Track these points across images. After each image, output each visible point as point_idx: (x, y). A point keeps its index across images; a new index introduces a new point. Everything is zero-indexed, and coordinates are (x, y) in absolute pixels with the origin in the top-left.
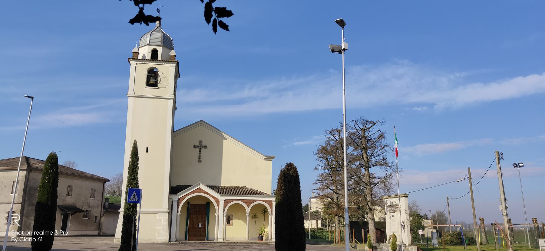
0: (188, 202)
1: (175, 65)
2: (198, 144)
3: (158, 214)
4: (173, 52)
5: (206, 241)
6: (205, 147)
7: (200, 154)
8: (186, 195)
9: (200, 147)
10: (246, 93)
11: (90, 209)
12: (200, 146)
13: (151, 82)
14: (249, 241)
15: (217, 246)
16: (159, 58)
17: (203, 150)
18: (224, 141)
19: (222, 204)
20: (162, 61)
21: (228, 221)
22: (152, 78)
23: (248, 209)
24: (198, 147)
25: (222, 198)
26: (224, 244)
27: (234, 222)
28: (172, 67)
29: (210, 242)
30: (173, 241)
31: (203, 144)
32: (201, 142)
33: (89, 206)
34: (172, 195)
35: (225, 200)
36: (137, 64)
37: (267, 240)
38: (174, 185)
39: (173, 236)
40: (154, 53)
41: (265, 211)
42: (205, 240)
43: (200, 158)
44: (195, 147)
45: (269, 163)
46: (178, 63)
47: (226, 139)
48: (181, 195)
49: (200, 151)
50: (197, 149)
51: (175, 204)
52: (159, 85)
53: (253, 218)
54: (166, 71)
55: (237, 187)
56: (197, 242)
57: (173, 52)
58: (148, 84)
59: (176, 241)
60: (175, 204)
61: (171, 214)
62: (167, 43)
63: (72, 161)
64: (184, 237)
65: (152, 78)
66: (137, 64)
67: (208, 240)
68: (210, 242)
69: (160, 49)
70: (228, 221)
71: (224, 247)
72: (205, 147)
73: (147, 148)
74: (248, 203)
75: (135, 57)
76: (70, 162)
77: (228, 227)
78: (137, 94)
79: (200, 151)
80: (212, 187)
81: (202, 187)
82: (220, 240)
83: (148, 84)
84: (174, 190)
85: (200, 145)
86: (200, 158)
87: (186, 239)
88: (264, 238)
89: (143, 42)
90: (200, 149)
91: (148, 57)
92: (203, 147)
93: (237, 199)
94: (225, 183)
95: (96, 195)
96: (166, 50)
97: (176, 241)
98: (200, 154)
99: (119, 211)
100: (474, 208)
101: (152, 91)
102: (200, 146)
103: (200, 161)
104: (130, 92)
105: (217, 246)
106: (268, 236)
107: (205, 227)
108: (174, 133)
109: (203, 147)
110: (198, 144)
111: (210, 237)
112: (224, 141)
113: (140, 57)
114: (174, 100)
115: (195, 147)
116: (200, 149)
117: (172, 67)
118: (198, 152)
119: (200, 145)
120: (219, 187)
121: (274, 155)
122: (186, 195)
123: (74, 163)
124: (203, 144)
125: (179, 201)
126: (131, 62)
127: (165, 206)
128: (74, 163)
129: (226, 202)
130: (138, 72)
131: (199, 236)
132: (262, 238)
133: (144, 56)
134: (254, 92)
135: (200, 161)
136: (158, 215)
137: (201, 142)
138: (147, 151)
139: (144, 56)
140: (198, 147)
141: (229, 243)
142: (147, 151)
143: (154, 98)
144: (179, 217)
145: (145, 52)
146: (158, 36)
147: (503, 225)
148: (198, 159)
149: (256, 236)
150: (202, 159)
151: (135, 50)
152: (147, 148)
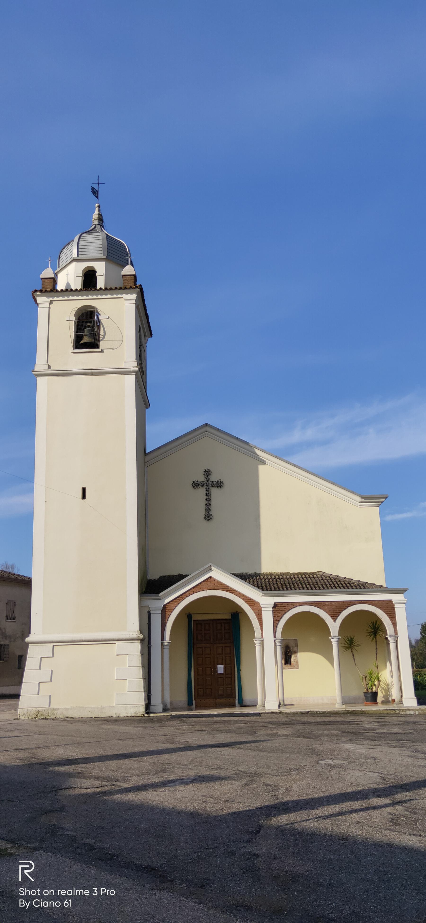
0: (187, 614)
1: (134, 296)
2: (202, 479)
3: (117, 645)
4: (129, 270)
5: (237, 710)
6: (219, 484)
7: (208, 500)
8: (179, 598)
9: (208, 485)
10: (296, 436)
11: (7, 642)
12: (208, 484)
14: (339, 707)
15: (266, 725)
16: (101, 283)
17: (214, 491)
18: (261, 468)
19: (268, 615)
20: (107, 290)
21: (287, 656)
22: (87, 332)
23: (334, 626)
24: (202, 485)
25: (268, 601)
26: (284, 719)
27: (302, 658)
28: (128, 301)
29: (246, 710)
30: (158, 713)
31: (214, 478)
32: (207, 473)
33: (5, 637)
34: (145, 597)
35: (275, 605)
36: (51, 302)
37: (387, 701)
38: (154, 575)
39: (157, 699)
40: (89, 279)
41: (376, 629)
42: (233, 705)
44: (196, 485)
45: (373, 513)
46: (141, 290)
47: (263, 463)
48: (169, 596)
49: (208, 495)
50: (202, 491)
51: (157, 620)
52: (102, 344)
54: (118, 314)
55: (298, 574)
56: (215, 712)
57: (129, 270)
58: (79, 344)
59: (165, 710)
60: (157, 620)
61: (146, 642)
62: (116, 254)
63: (10, 563)
64: (182, 698)
65: (87, 332)
66: (51, 302)
67: (242, 705)
68: (246, 710)
69: (100, 268)
70: (287, 656)
71: (282, 731)
72: (219, 484)
73: (84, 490)
74: (334, 609)
75: (50, 288)
76: (7, 564)
77: (288, 672)
78: (55, 367)
79: (208, 495)
80: (243, 577)
81: (217, 574)
82: (272, 706)
83: (79, 344)
84: (151, 586)
85: (208, 479)
87: (190, 703)
88: (380, 698)
89: (64, 258)
90: (208, 490)
91: (77, 284)
92: (213, 485)
93: (304, 601)
94: (269, 566)
95: (17, 614)
96: (114, 268)
97: (165, 710)
98: (208, 500)
99: (27, 640)
100: (377, 652)
101: (87, 359)
102: (208, 484)
103: (208, 517)
104: (40, 365)
105: (266, 725)
106: (387, 690)
107: (232, 673)
108: (148, 458)
109: (213, 485)
110: (202, 479)
111: (247, 697)
112: (261, 468)
113: (59, 287)
114: (141, 374)
115: (196, 485)
116: (208, 490)
117: (128, 301)
119: (208, 479)
120: (257, 575)
121: (385, 494)
122: (179, 598)
123: (13, 566)
124: (214, 478)
125: (165, 612)
126: (39, 299)
127: (132, 626)
128: (13, 566)
129: (279, 610)
130: (56, 319)
131: (221, 696)
132: (373, 697)
133: (68, 284)
134: (310, 433)
135: (208, 517)
136: (116, 647)
137: (207, 473)
138: (84, 497)
139: (68, 284)
140: (202, 485)
141: (295, 714)
142: (84, 497)
143: (92, 374)
144: (166, 651)
145: (70, 276)
146: (95, 243)
148: (203, 512)
149: (358, 692)
151: (48, 273)
152: (84, 490)
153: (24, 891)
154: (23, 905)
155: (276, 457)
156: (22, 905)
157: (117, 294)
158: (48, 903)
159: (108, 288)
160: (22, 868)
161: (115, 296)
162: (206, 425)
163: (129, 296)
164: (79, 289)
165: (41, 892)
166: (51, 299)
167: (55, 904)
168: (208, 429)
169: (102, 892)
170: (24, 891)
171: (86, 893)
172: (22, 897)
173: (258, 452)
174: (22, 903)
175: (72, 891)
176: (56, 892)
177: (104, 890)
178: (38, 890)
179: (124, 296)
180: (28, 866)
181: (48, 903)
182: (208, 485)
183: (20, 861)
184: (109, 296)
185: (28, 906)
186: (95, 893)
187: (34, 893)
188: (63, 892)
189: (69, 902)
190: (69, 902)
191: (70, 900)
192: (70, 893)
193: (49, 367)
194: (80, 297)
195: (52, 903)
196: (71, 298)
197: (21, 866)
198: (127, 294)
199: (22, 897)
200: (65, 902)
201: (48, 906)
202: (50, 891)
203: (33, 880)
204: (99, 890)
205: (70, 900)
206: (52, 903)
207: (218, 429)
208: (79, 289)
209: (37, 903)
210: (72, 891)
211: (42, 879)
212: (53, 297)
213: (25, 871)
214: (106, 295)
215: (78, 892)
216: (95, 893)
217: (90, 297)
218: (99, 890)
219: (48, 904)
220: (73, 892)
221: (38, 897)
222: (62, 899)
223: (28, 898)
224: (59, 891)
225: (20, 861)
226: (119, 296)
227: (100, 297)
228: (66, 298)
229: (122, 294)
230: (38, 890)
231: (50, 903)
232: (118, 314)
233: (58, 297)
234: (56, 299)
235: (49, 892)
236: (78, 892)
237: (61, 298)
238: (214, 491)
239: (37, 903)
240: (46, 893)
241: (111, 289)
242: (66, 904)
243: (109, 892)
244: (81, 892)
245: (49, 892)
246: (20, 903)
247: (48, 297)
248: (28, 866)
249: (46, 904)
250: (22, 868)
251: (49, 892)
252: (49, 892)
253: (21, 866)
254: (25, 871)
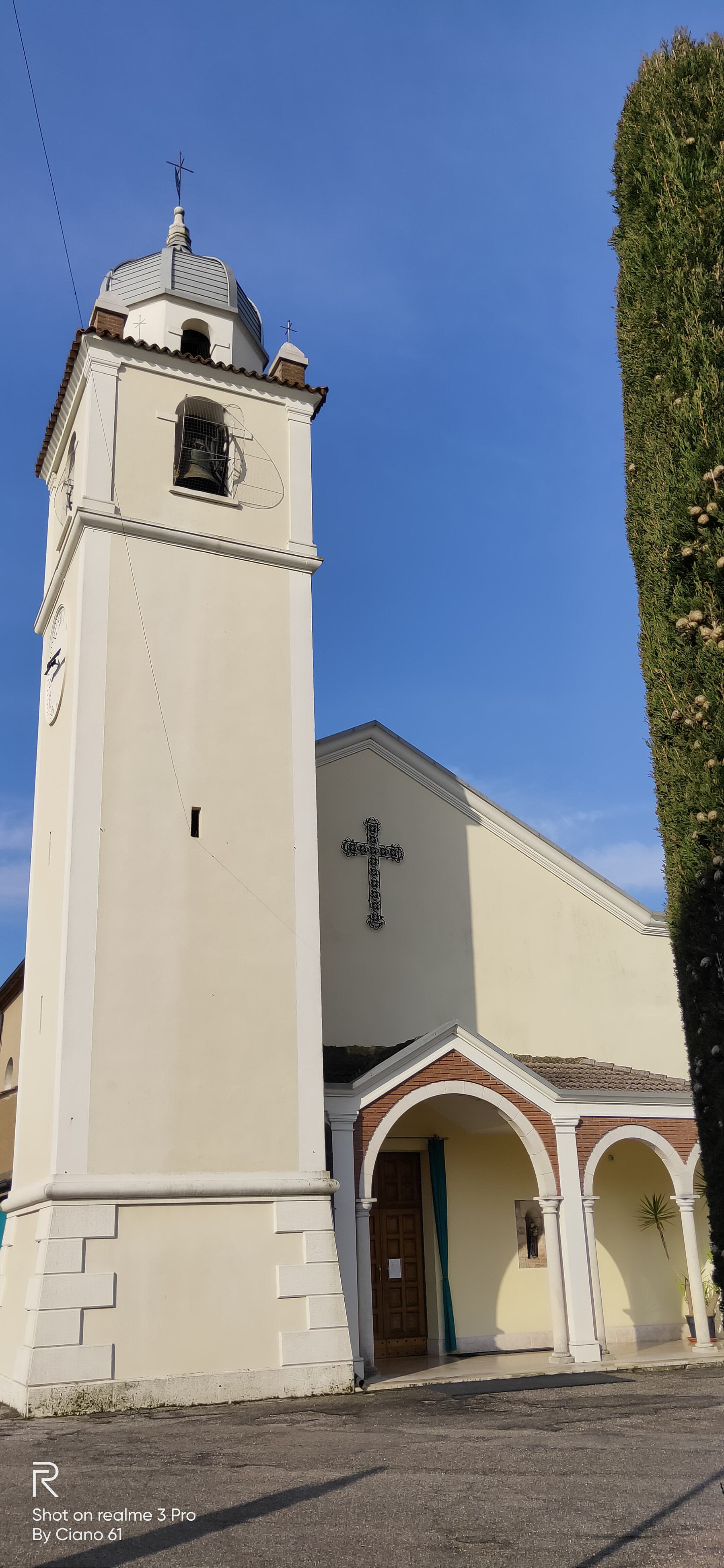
2: (360, 837)
6: (395, 854)
7: (374, 884)
9: (373, 851)
13: (196, 472)
17: (385, 866)
22: (203, 454)
25: (565, 1113)
31: (385, 840)
32: (372, 827)
36: (122, 368)
43: (375, 906)
47: (477, 821)
49: (373, 873)
50: (360, 864)
53: (647, 1222)
54: (273, 434)
65: (203, 454)
66: (122, 368)
72: (395, 854)
75: (109, 330)
78: (132, 512)
79: (373, 873)
84: (344, 1066)
86: (375, 906)
90: (373, 863)
98: (374, 884)
101: (195, 514)
103: (375, 921)
110: (360, 837)
116: (373, 863)
118: (365, 879)
122: (394, 1096)
124: (385, 840)
129: (588, 1131)
135: (375, 921)
136: (277, 1213)
140: (362, 850)
147: (404, 1239)
150: (383, 912)
152: (195, 813)
153: (41, 1513)
154: (39, 1537)
155: (506, 814)
156: (37, 1537)
157: (272, 393)
158: (81, 1533)
159: (237, 368)
160: (37, 1474)
161: (266, 396)
162: (375, 724)
163: (297, 405)
164: (172, 350)
165: (70, 1516)
166: (122, 360)
167: (93, 1536)
168: (376, 733)
169: (173, 1515)
170: (40, 1514)
171: (147, 1516)
172: (38, 1525)
173: (470, 797)
174: (38, 1534)
175: (122, 1514)
176: (96, 1515)
177: (176, 1512)
178: (65, 1513)
179: (287, 401)
180: (47, 1471)
181: (81, 1533)
182: (373, 851)
183: (34, 1463)
184: (254, 392)
185: (47, 1539)
186: (162, 1517)
187: (57, 1516)
188: (106, 1516)
189: (118, 1533)
190: (118, 1533)
191: (120, 1529)
192: (118, 1516)
193: (117, 510)
194: (190, 376)
195: (88, 1535)
196: (169, 371)
197: (35, 1472)
198: (293, 398)
199: (38, 1525)
200: (111, 1533)
201: (81, 1538)
202: (85, 1514)
203: (56, 1495)
204: (168, 1513)
205: (120, 1529)
206: (88, 1535)
207: (399, 737)
208: (172, 350)
209: (63, 1534)
210: (122, 1514)
211: (69, 1496)
212: (129, 356)
213: (43, 1480)
214: (249, 387)
215: (132, 1516)
216: (162, 1517)
217: (212, 382)
218: (168, 1513)
219: (83, 1536)
220: (124, 1515)
221: (65, 1524)
222: (106, 1527)
223: (48, 1526)
224: (100, 1514)
225: (34, 1463)
226: (277, 398)
227: (234, 388)
228: (157, 368)
229: (283, 396)
230: (65, 1513)
231: (85, 1533)
232: (273, 434)
233: (140, 359)
234: (133, 362)
235: (83, 1516)
236: (132, 1516)
237: (145, 365)
238: (385, 866)
239: (63, 1534)
240: (78, 1516)
241: (242, 371)
242: (112, 1536)
243: (185, 1515)
244: (138, 1515)
245: (83, 1516)
246: (34, 1534)
247: (117, 353)
248: (47, 1471)
249: (77, 1536)
250: (37, 1474)
251: (83, 1516)
252: (83, 1516)
253: (35, 1472)
254: (43, 1480)
